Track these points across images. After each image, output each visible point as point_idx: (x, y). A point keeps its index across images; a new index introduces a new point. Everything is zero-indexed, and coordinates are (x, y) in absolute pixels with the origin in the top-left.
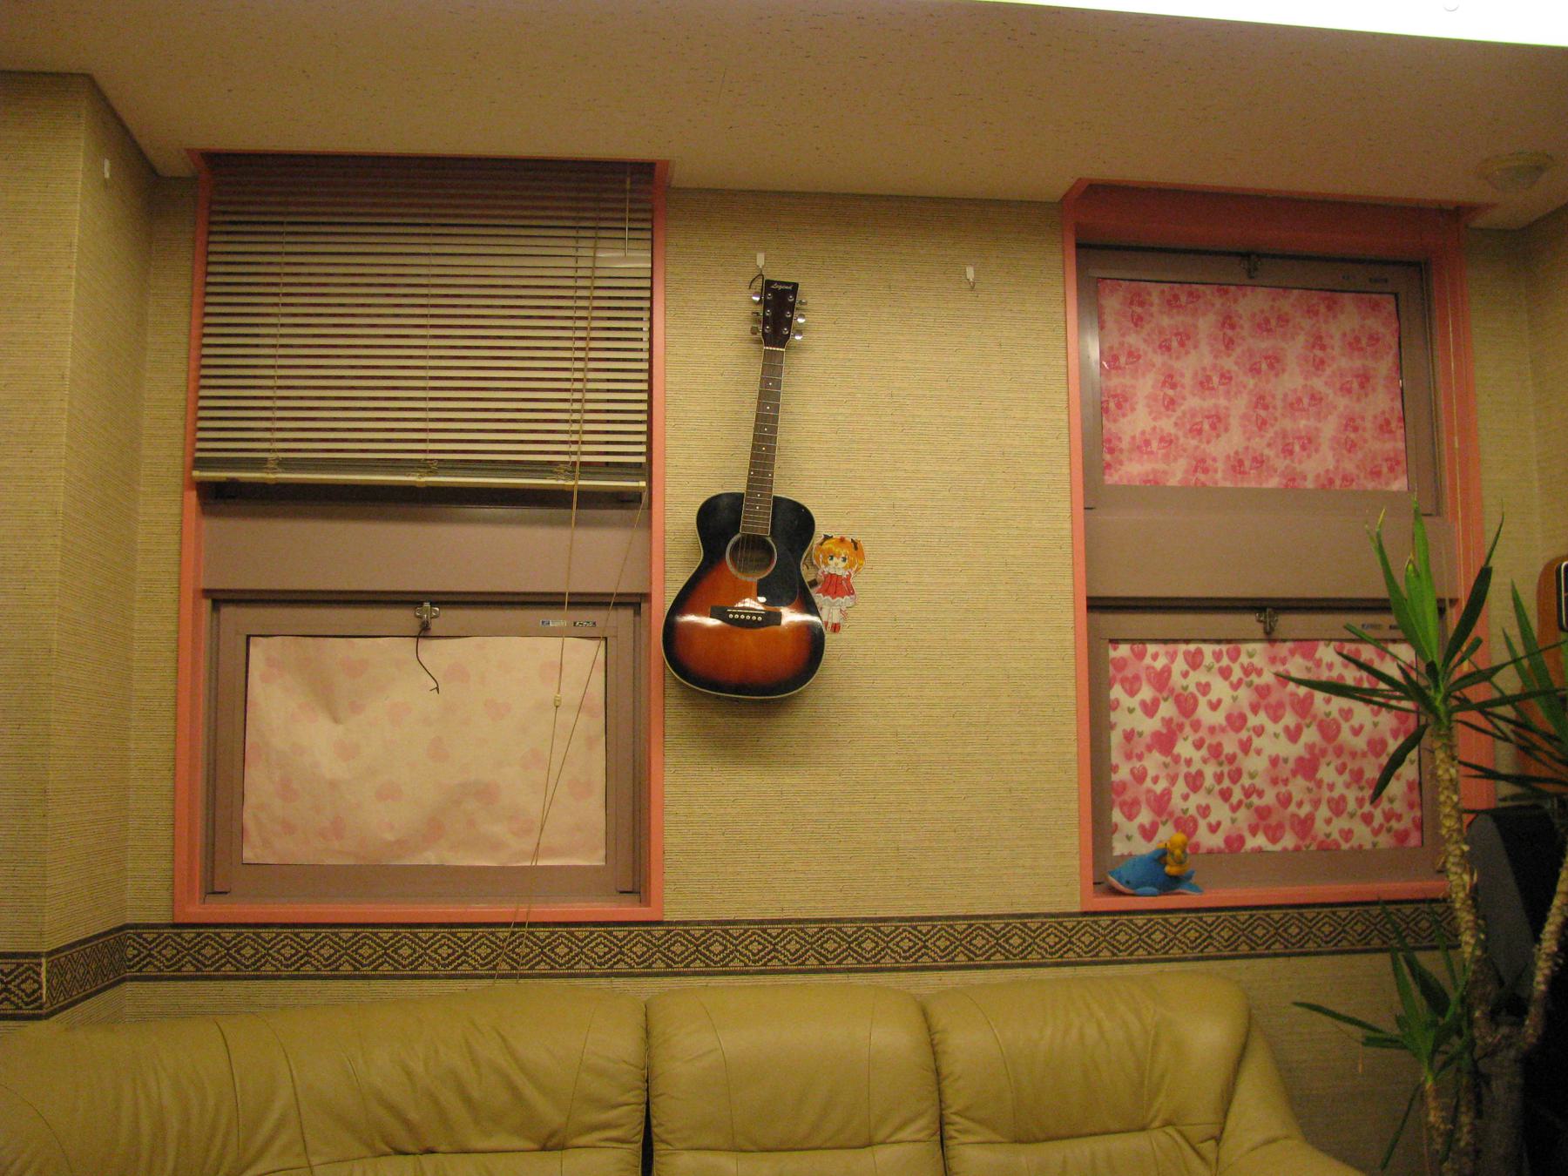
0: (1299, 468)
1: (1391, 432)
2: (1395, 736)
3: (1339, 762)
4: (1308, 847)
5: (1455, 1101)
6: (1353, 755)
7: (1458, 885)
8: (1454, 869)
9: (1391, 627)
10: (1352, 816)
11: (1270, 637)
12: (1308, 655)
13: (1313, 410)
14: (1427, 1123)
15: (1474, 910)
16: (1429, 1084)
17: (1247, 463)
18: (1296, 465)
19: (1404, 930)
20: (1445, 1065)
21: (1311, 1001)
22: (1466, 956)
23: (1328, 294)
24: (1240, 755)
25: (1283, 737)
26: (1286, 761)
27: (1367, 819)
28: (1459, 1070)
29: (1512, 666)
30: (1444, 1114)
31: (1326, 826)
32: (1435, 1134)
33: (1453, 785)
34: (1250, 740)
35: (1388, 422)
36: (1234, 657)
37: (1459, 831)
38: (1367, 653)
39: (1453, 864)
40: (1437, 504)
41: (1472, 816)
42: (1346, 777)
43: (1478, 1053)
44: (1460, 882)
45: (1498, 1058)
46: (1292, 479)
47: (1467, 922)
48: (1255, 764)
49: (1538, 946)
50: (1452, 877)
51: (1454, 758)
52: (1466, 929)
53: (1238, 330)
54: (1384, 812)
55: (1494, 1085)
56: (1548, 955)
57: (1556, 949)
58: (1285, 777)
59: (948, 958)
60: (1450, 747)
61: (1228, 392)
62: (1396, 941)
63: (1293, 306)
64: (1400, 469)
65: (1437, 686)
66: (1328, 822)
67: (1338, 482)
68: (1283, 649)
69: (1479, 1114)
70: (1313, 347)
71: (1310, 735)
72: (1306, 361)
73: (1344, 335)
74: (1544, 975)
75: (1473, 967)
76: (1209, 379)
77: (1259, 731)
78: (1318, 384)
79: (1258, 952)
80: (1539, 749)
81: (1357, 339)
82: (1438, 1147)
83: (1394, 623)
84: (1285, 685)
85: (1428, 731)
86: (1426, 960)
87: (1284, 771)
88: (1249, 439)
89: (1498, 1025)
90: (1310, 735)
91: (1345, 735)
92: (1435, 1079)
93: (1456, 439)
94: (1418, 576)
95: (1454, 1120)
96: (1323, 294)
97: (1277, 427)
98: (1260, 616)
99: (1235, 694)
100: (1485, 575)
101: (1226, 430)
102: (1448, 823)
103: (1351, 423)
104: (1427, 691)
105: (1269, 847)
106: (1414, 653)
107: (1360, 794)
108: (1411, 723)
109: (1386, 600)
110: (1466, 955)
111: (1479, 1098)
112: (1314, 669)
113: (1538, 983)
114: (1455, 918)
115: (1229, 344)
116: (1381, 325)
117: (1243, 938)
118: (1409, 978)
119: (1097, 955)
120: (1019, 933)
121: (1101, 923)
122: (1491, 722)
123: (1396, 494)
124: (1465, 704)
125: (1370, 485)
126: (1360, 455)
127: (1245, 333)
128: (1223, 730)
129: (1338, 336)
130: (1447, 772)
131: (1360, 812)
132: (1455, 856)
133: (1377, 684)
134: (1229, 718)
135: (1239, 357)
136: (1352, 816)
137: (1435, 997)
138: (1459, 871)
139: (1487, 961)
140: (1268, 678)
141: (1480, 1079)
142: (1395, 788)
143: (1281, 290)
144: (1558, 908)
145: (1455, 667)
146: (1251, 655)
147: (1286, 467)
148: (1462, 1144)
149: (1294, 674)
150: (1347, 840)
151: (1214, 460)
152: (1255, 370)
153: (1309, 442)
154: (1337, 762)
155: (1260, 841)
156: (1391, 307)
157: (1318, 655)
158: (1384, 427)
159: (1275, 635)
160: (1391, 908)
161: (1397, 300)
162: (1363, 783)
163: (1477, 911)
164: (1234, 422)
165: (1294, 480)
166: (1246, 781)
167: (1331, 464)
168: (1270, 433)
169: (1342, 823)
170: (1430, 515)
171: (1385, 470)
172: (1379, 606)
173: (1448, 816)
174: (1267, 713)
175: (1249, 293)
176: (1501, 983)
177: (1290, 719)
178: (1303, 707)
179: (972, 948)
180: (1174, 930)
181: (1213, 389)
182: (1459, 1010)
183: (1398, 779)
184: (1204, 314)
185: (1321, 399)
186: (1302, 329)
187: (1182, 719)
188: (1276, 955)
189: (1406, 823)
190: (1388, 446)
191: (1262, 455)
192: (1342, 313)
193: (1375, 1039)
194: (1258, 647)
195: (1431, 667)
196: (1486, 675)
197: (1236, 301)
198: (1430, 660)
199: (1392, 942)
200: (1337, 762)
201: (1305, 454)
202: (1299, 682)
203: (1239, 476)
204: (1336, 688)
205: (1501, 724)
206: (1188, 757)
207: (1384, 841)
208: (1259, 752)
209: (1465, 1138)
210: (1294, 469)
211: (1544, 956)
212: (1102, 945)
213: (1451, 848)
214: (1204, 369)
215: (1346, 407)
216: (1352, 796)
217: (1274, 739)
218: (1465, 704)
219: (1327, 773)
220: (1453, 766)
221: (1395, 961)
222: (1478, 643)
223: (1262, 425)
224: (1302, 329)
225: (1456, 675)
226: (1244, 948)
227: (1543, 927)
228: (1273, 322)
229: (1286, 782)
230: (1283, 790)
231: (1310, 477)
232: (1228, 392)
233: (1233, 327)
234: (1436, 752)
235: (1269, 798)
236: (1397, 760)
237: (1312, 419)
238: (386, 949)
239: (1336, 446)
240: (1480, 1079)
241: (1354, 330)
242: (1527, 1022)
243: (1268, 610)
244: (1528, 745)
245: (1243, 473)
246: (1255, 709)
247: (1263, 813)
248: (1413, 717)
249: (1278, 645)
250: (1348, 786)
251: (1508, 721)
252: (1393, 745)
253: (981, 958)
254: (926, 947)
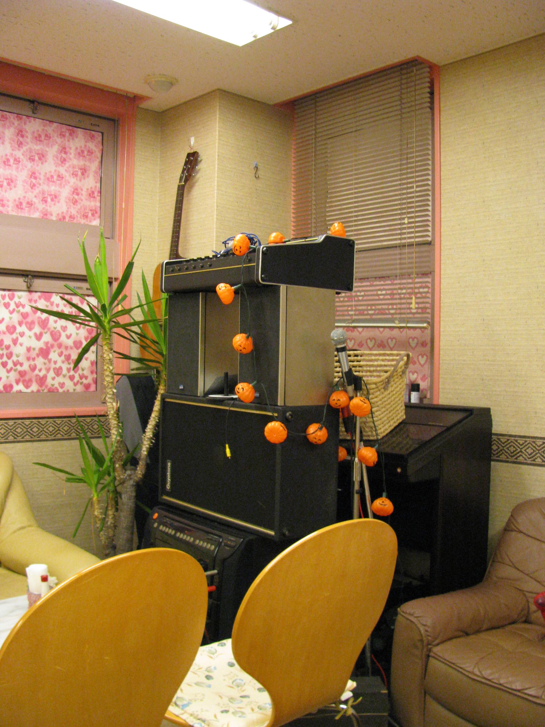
0: (49, 210)
1: (94, 197)
2: (86, 340)
3: (60, 351)
4: (43, 390)
5: (106, 505)
6: (66, 348)
7: (111, 408)
8: (109, 400)
9: (87, 289)
10: (64, 376)
11: (30, 290)
12: (48, 299)
13: (58, 182)
14: (94, 515)
15: (117, 419)
16: (95, 498)
17: (24, 205)
18: (48, 208)
19: (87, 429)
20: (102, 489)
21: (43, 462)
22: (113, 440)
23: (71, 128)
24: (12, 345)
25: (34, 338)
26: (34, 349)
27: (72, 378)
28: (108, 491)
29: (139, 309)
30: (101, 511)
31: (52, 381)
32: (97, 520)
33: (111, 362)
34: (17, 339)
35: (93, 193)
36: (12, 298)
37: (112, 383)
38: (76, 300)
39: (109, 398)
40: (113, 233)
41: (120, 376)
42: (63, 358)
43: (117, 483)
44: (112, 406)
45: (125, 485)
46: (45, 214)
47: (115, 424)
48: (19, 351)
49: (144, 435)
50: (108, 404)
51: (111, 349)
52: (114, 427)
53: (25, 138)
54: (79, 375)
55: (123, 496)
56: (148, 438)
57: (152, 436)
58: (33, 357)
59: (5, 438)
60: (110, 344)
61: (17, 168)
62: (83, 434)
63: (54, 131)
64: (97, 215)
65: (106, 316)
66: (53, 379)
67: (67, 219)
68: (36, 296)
69: (117, 510)
70: (61, 152)
71: (47, 338)
72: (57, 158)
73: (77, 148)
74: (147, 447)
75: (116, 445)
76: (8, 160)
77: (22, 334)
78: (62, 170)
79: (18, 440)
80: (150, 347)
81: (83, 152)
82: (98, 525)
83: (89, 287)
84: (35, 313)
85: (101, 337)
86: (95, 442)
87: (33, 354)
88: (26, 192)
89: (126, 470)
90: (47, 338)
91: (63, 339)
92: (98, 495)
93: (124, 204)
94: (100, 264)
95: (106, 514)
96: (68, 127)
97: (40, 189)
98: (25, 279)
99: (11, 316)
100: (130, 265)
101: (15, 187)
102: (108, 379)
103: (76, 191)
104: (101, 318)
105: (24, 390)
106: (97, 301)
107: (69, 366)
108: (94, 334)
109: (85, 276)
110: (113, 440)
111: (117, 503)
112: (50, 306)
113: (144, 451)
114: (109, 424)
115: (20, 144)
116: (94, 146)
117: (11, 433)
118: (88, 451)
119: (70, 436)
120: (37, 426)
121: (9, 423)
122: (129, 334)
123: (94, 227)
124: (117, 325)
125: (83, 221)
126: (79, 207)
127: (29, 140)
128: (71, 348)
129: (73, 148)
130: (108, 355)
131: (68, 375)
132: (110, 394)
133: (80, 314)
134: (8, 327)
135: (24, 152)
136: (64, 376)
137: (99, 459)
138: (112, 401)
139: (122, 442)
140: (28, 309)
141: (117, 494)
142: (85, 364)
143: (48, 122)
144: (154, 418)
145: (115, 307)
146: (20, 298)
147: (43, 208)
148: (109, 523)
149: (40, 307)
150: (62, 387)
151: (8, 201)
152: (32, 159)
153: (55, 197)
154: (58, 351)
155: (20, 387)
156: (100, 139)
157: (52, 300)
158: (91, 195)
159: (32, 289)
160: (81, 419)
161: (103, 135)
162: (71, 361)
163: (119, 420)
164: (20, 183)
165: (46, 215)
166: (14, 358)
167: (64, 209)
168: (37, 191)
169: (60, 379)
170: (109, 238)
171: (90, 215)
172: (82, 279)
173: (108, 376)
174: (26, 326)
175: (32, 121)
176: (128, 451)
177: (37, 329)
178: (44, 324)
179: (16, 433)
180: (43, 427)
181: (10, 165)
182: (109, 464)
183: (86, 359)
184: (9, 128)
185: (63, 178)
186: (57, 143)
187: (54, 342)
188: (27, 441)
189: (89, 380)
190: (93, 204)
191: (32, 201)
192: (77, 137)
193: (73, 479)
194: (24, 294)
195: (103, 307)
196: (127, 312)
197: (25, 124)
198: (103, 303)
199: (81, 435)
200: (58, 351)
201: (53, 203)
202: (43, 311)
203: (20, 210)
204: (60, 315)
205: (133, 334)
206: (55, 360)
207: (79, 388)
208: (21, 345)
209: (110, 521)
210: (47, 210)
211: (146, 439)
212: (10, 434)
213: (109, 391)
214: (6, 155)
215: (74, 183)
216: (65, 366)
217: (29, 338)
218: (117, 325)
219: (54, 355)
220: (111, 353)
221: (81, 444)
222: (125, 297)
223: (33, 186)
224: (57, 143)
225: (115, 311)
226: (11, 438)
227: (147, 426)
228: (43, 137)
229: (34, 359)
230: (32, 363)
231: (54, 214)
232: (17, 168)
233: (22, 136)
234: (104, 347)
235: (26, 367)
236: (86, 350)
237: (58, 187)
238: (27, 429)
239: (68, 201)
240: (117, 494)
241: (81, 147)
242: (138, 468)
243: (29, 276)
244: (145, 345)
245: (22, 209)
246: (20, 324)
247: (22, 374)
248: (95, 329)
249: (34, 294)
250: (63, 362)
251: (136, 333)
252: (85, 343)
253: (20, 438)
254: (59, 430)
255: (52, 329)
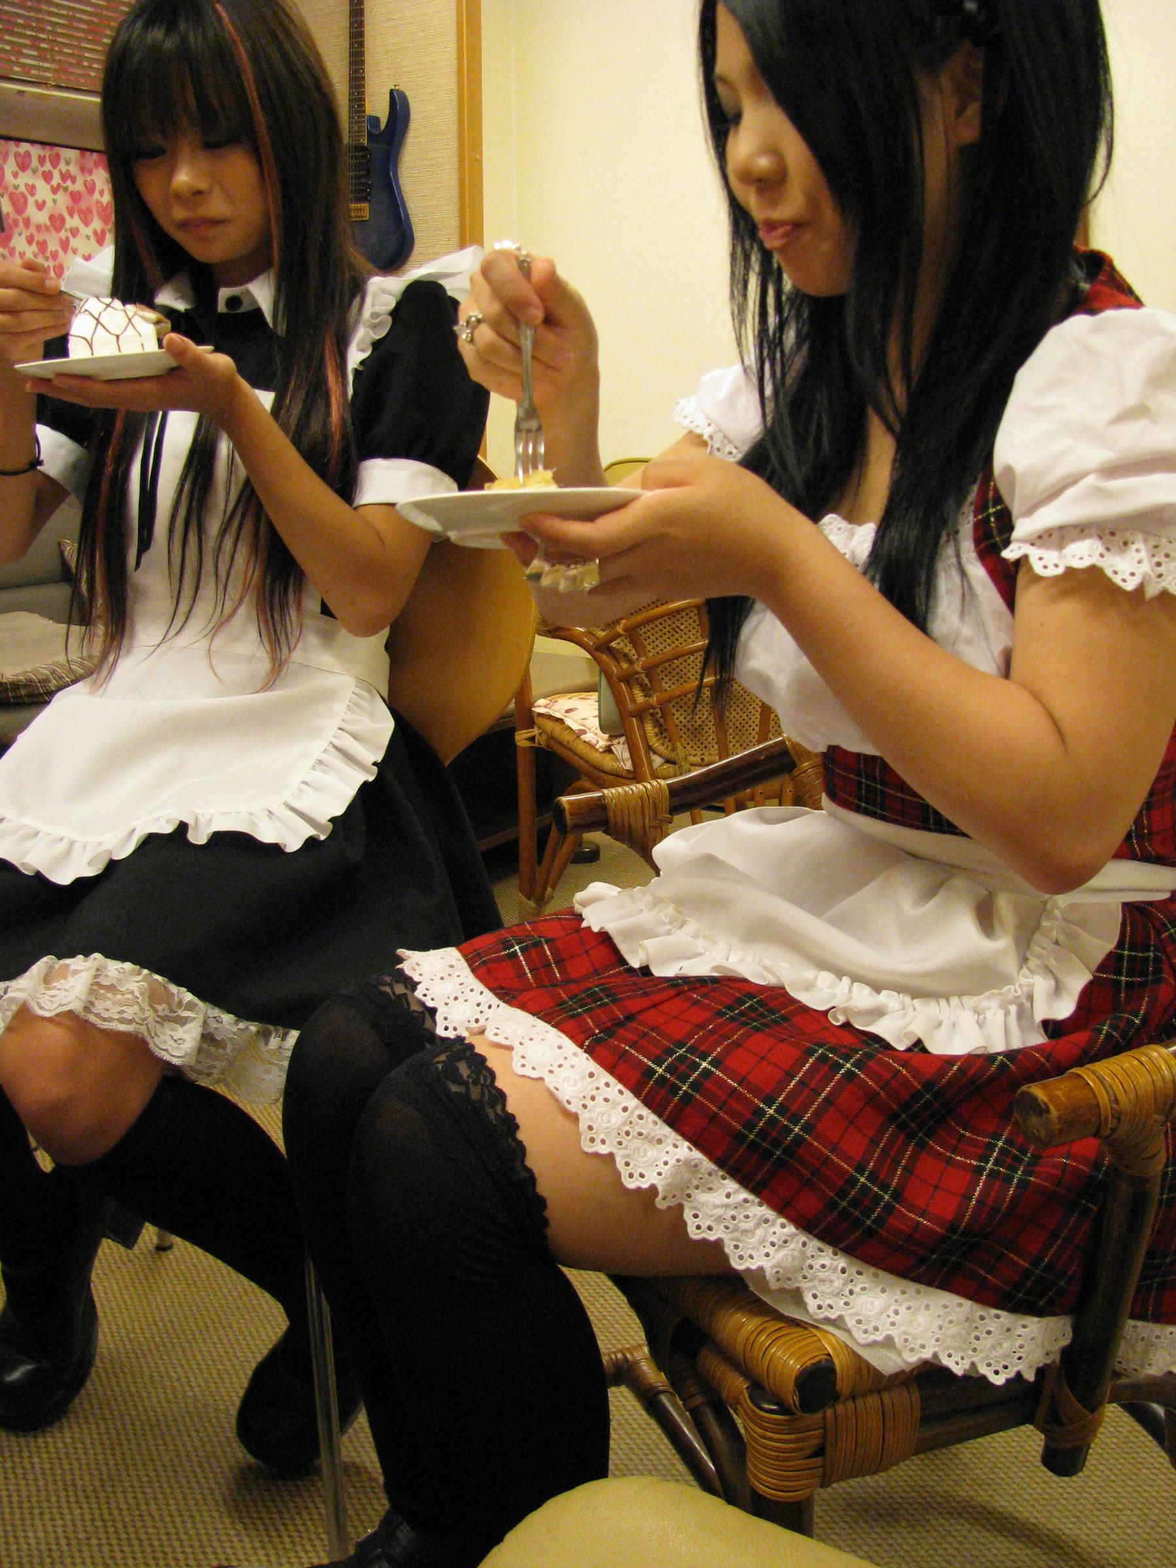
24: (61, 252)
34: (67, 239)
36: (55, 161)
77: (75, 232)
91: (31, 211)
200: (26, 233)
255: (11, 189)
